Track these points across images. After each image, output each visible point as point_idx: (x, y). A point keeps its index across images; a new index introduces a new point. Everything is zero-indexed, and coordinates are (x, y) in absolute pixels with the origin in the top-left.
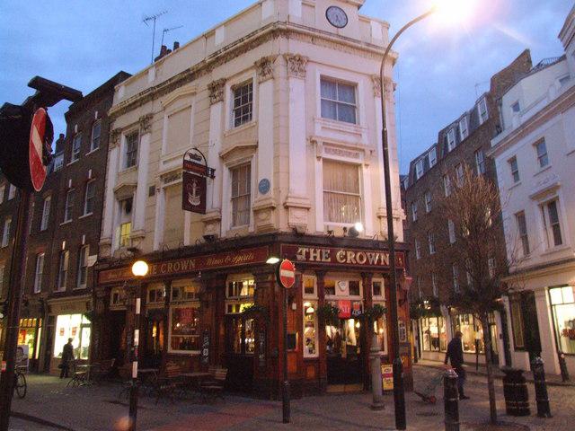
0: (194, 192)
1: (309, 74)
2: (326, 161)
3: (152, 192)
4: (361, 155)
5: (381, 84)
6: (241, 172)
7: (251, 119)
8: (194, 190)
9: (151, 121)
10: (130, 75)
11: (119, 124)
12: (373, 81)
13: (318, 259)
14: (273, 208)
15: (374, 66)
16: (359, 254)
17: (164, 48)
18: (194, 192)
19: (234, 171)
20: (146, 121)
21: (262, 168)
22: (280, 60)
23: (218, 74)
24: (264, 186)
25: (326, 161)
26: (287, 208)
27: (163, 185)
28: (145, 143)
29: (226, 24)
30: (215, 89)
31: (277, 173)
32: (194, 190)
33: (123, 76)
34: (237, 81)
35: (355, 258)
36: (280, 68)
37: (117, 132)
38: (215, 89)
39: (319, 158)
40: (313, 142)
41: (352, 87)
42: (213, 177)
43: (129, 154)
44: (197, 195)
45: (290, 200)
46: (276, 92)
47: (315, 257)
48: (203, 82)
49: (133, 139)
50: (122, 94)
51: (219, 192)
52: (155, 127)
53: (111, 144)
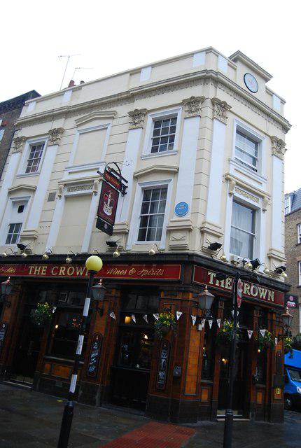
0: (109, 203)
1: (228, 121)
2: (236, 201)
3: (51, 197)
4: (260, 200)
5: (279, 145)
6: (154, 197)
7: (172, 145)
8: (109, 200)
9: (59, 136)
10: (39, 96)
11: (25, 132)
12: (272, 142)
13: (222, 286)
14: (190, 230)
15: (275, 131)
16: (252, 287)
17: (72, 83)
18: (109, 203)
19: (146, 193)
20: (55, 133)
21: (179, 192)
22: (208, 103)
23: (139, 104)
24: (182, 209)
25: (236, 201)
26: (203, 232)
27: (66, 193)
28: (49, 154)
29: (153, 66)
30: (137, 115)
31: (27, 221)
32: (109, 200)
33: (34, 94)
34: (159, 114)
35: (250, 290)
36: (207, 110)
37: (24, 139)
38: (137, 115)
39: (230, 194)
40: (228, 180)
41: (257, 143)
42: (124, 193)
43: (30, 162)
44: (110, 206)
45: (207, 225)
46: (202, 128)
47: (37, 272)
48: (123, 110)
49: (37, 149)
50: (30, 110)
51: (129, 211)
52: (65, 140)
53: (12, 150)
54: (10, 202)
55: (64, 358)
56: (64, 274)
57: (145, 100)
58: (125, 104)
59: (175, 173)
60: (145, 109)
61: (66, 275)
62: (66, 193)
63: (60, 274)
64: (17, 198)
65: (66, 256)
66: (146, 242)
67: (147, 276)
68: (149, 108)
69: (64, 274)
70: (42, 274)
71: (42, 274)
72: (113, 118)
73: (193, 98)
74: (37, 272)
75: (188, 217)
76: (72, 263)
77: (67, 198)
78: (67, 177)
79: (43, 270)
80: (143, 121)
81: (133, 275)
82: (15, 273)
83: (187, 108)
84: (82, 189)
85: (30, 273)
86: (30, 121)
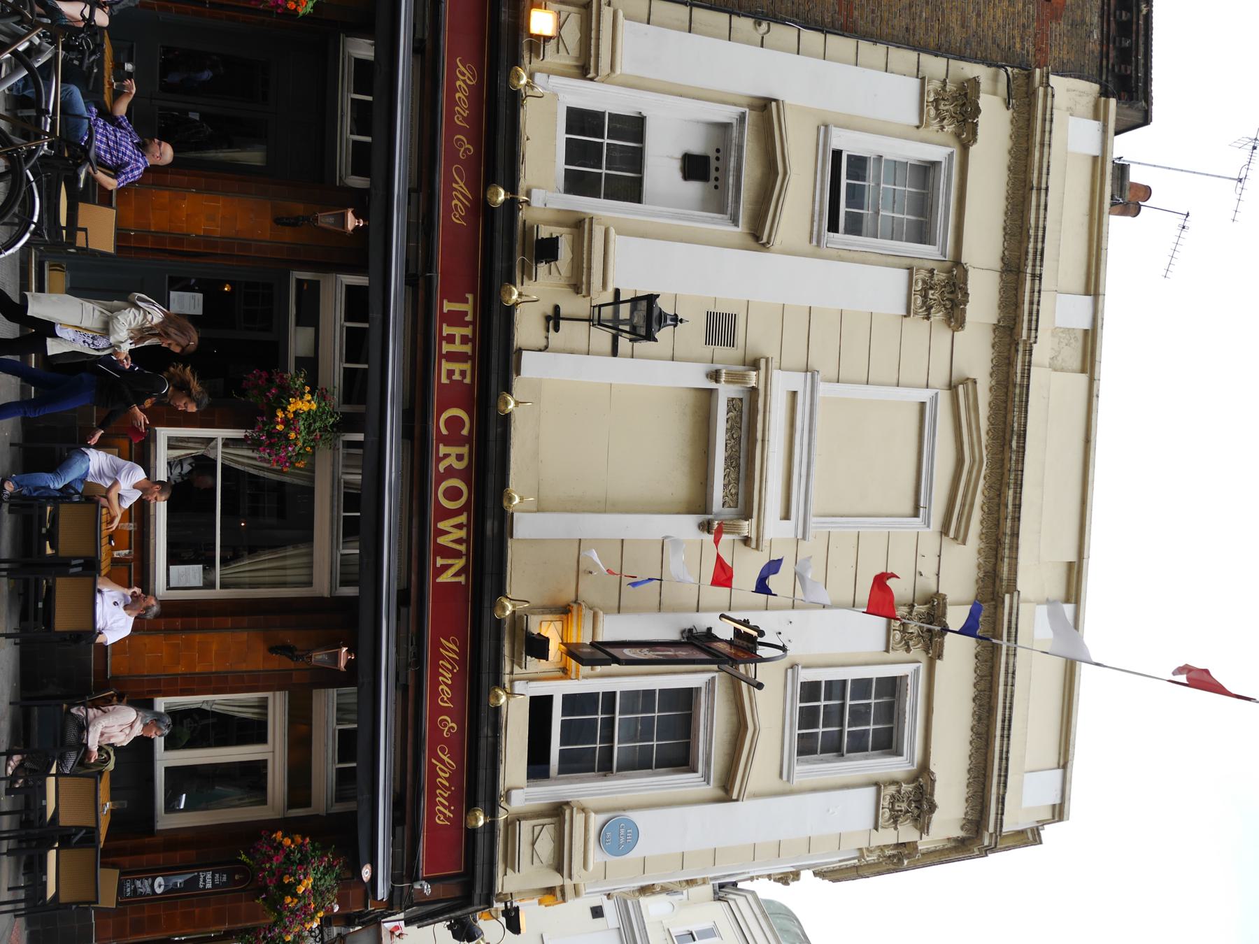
9: (938, 316)
10: (1117, 133)
34: (913, 703)
45: (579, 819)
47: (451, 339)
54: (726, 114)
55: (135, 516)
56: (442, 467)
57: (965, 782)
58: (979, 566)
59: (758, 236)
60: (940, 656)
61: (441, 478)
62: (726, 392)
63: (443, 450)
64: (711, 708)
65: (512, 187)
66: (562, 137)
67: (434, 774)
68: (973, 150)
69: (442, 467)
70: (446, 366)
71: (446, 366)
72: (945, 531)
73: (933, 807)
74: (451, 339)
75: (596, 856)
76: (472, 833)
77: (708, 395)
78: (781, 384)
79: (457, 367)
80: (942, 128)
81: (435, 730)
82: (432, 824)
83: (940, 276)
84: (728, 459)
85: (448, 306)
86: (1028, 152)
